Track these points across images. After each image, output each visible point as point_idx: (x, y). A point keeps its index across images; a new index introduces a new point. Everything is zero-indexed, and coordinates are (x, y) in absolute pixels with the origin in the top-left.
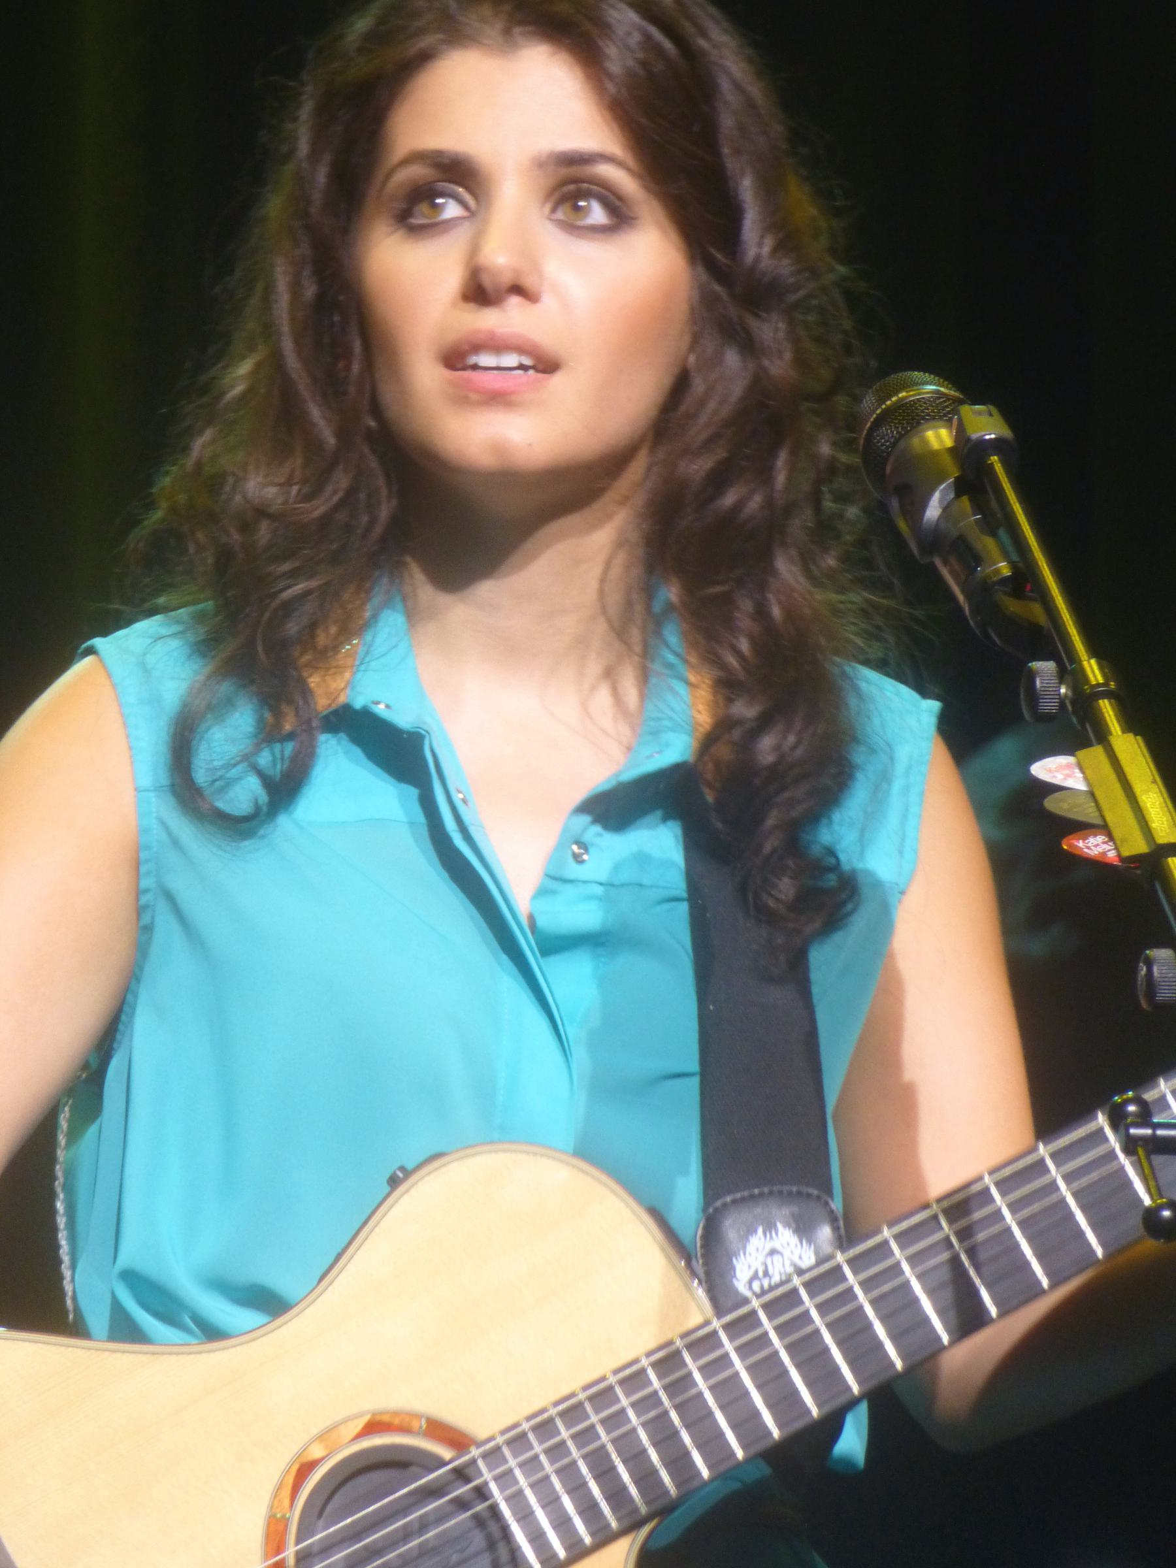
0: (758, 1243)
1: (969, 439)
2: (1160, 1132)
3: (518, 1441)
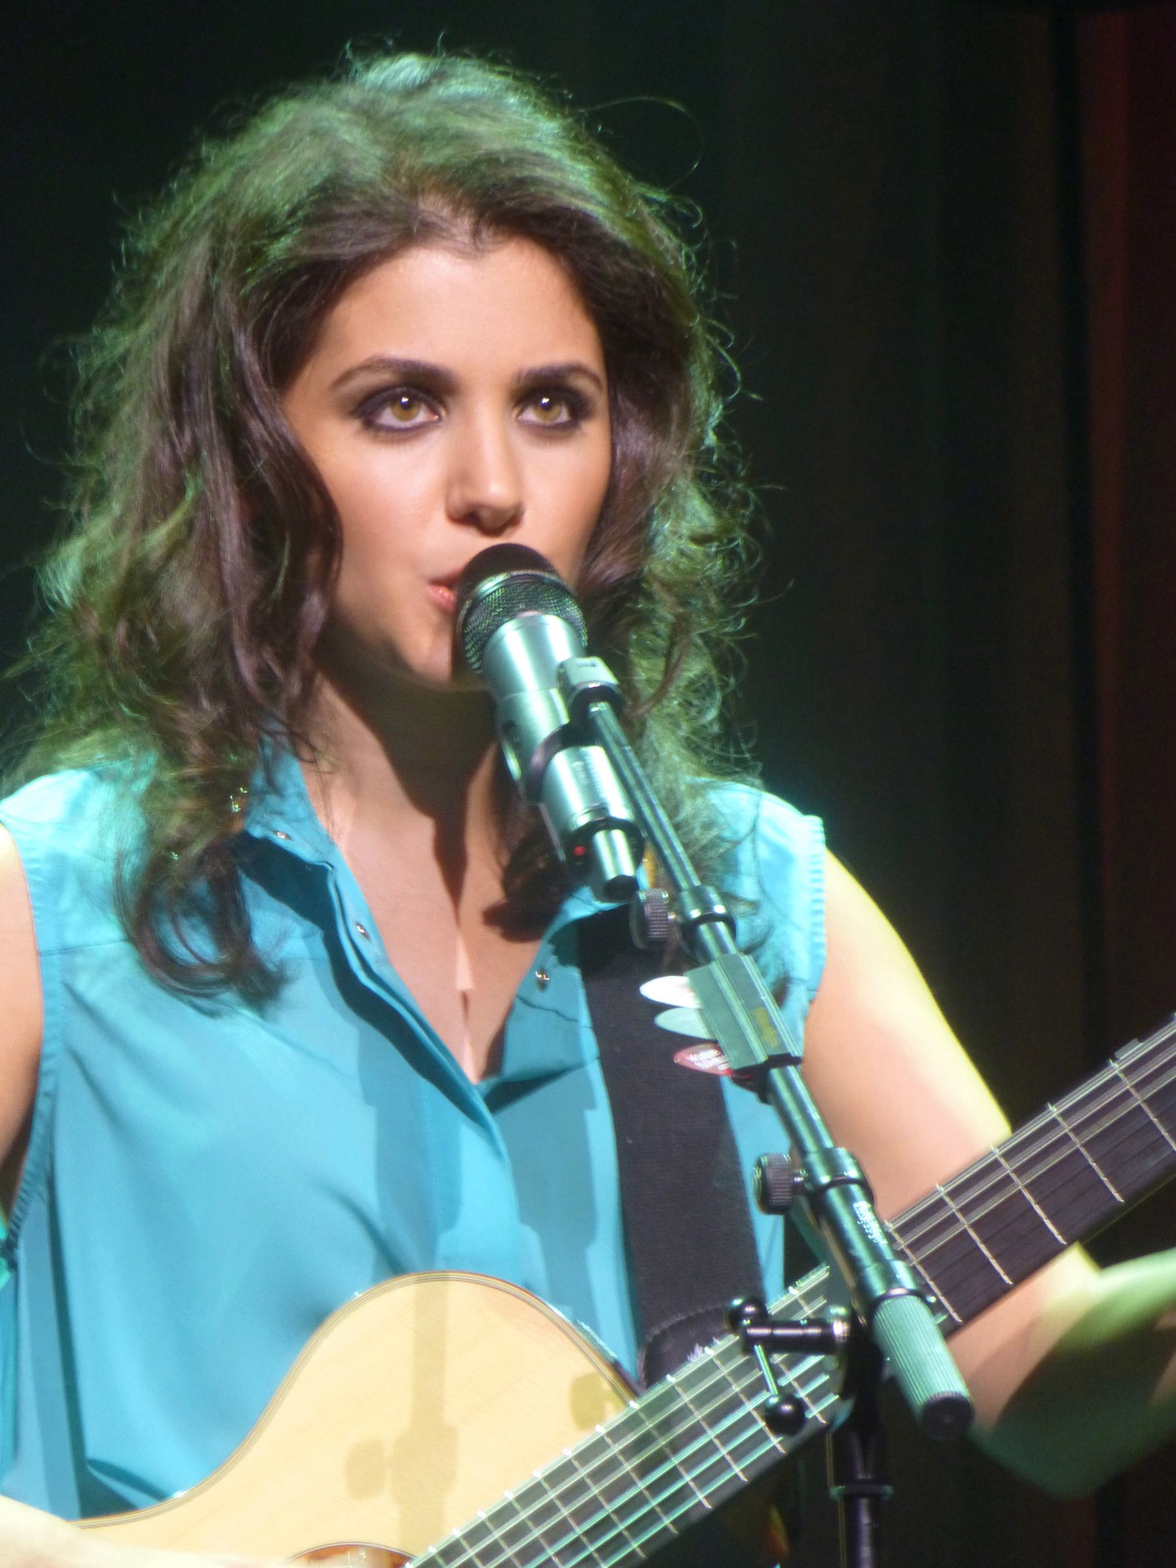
2: (779, 1332)
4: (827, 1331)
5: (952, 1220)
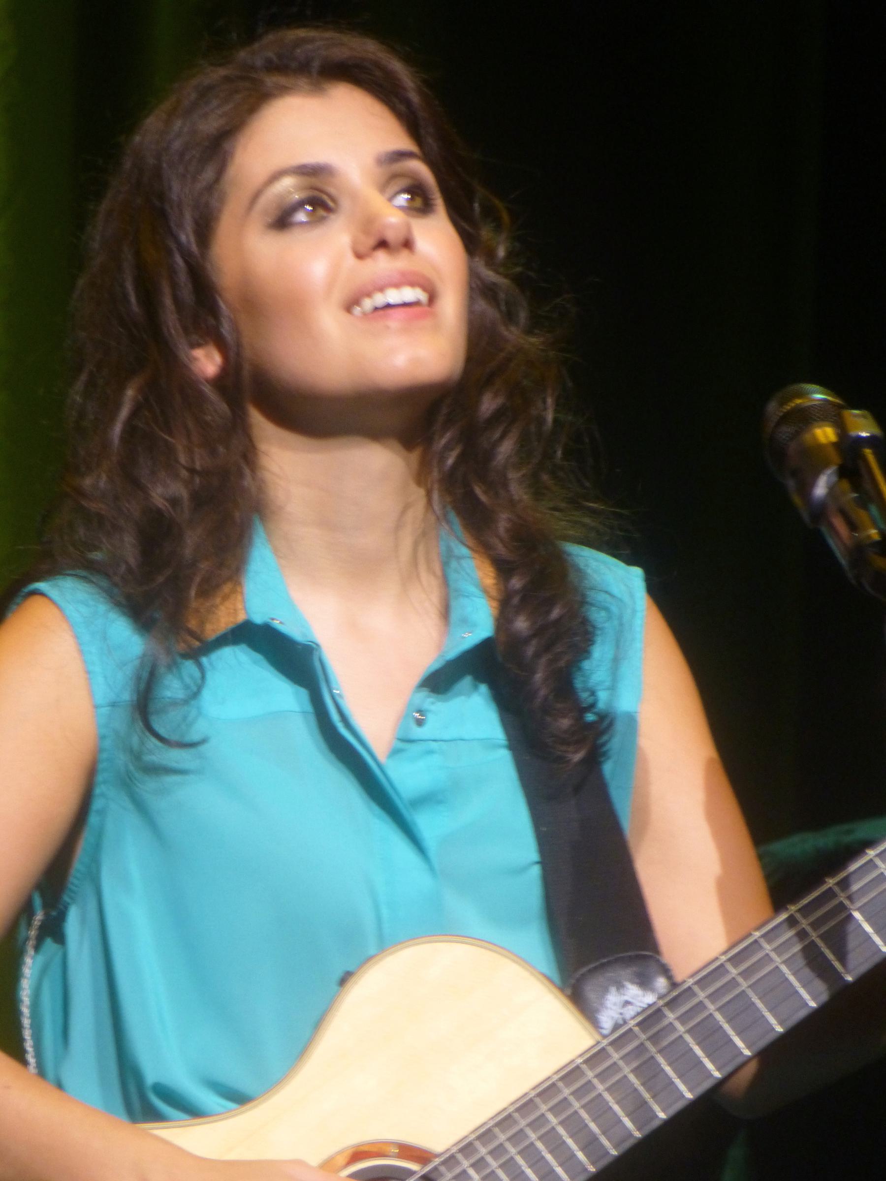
0: (613, 999)
1: (849, 437)
3: (467, 1148)
5: (733, 983)
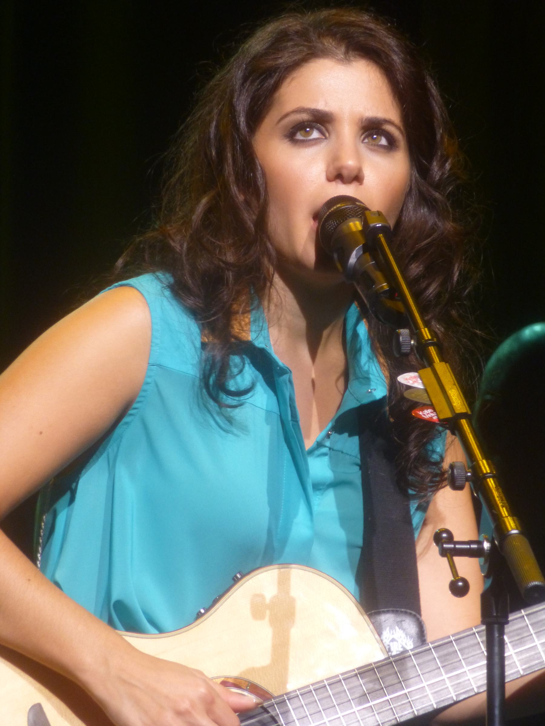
2: (457, 546)
4: (481, 546)
